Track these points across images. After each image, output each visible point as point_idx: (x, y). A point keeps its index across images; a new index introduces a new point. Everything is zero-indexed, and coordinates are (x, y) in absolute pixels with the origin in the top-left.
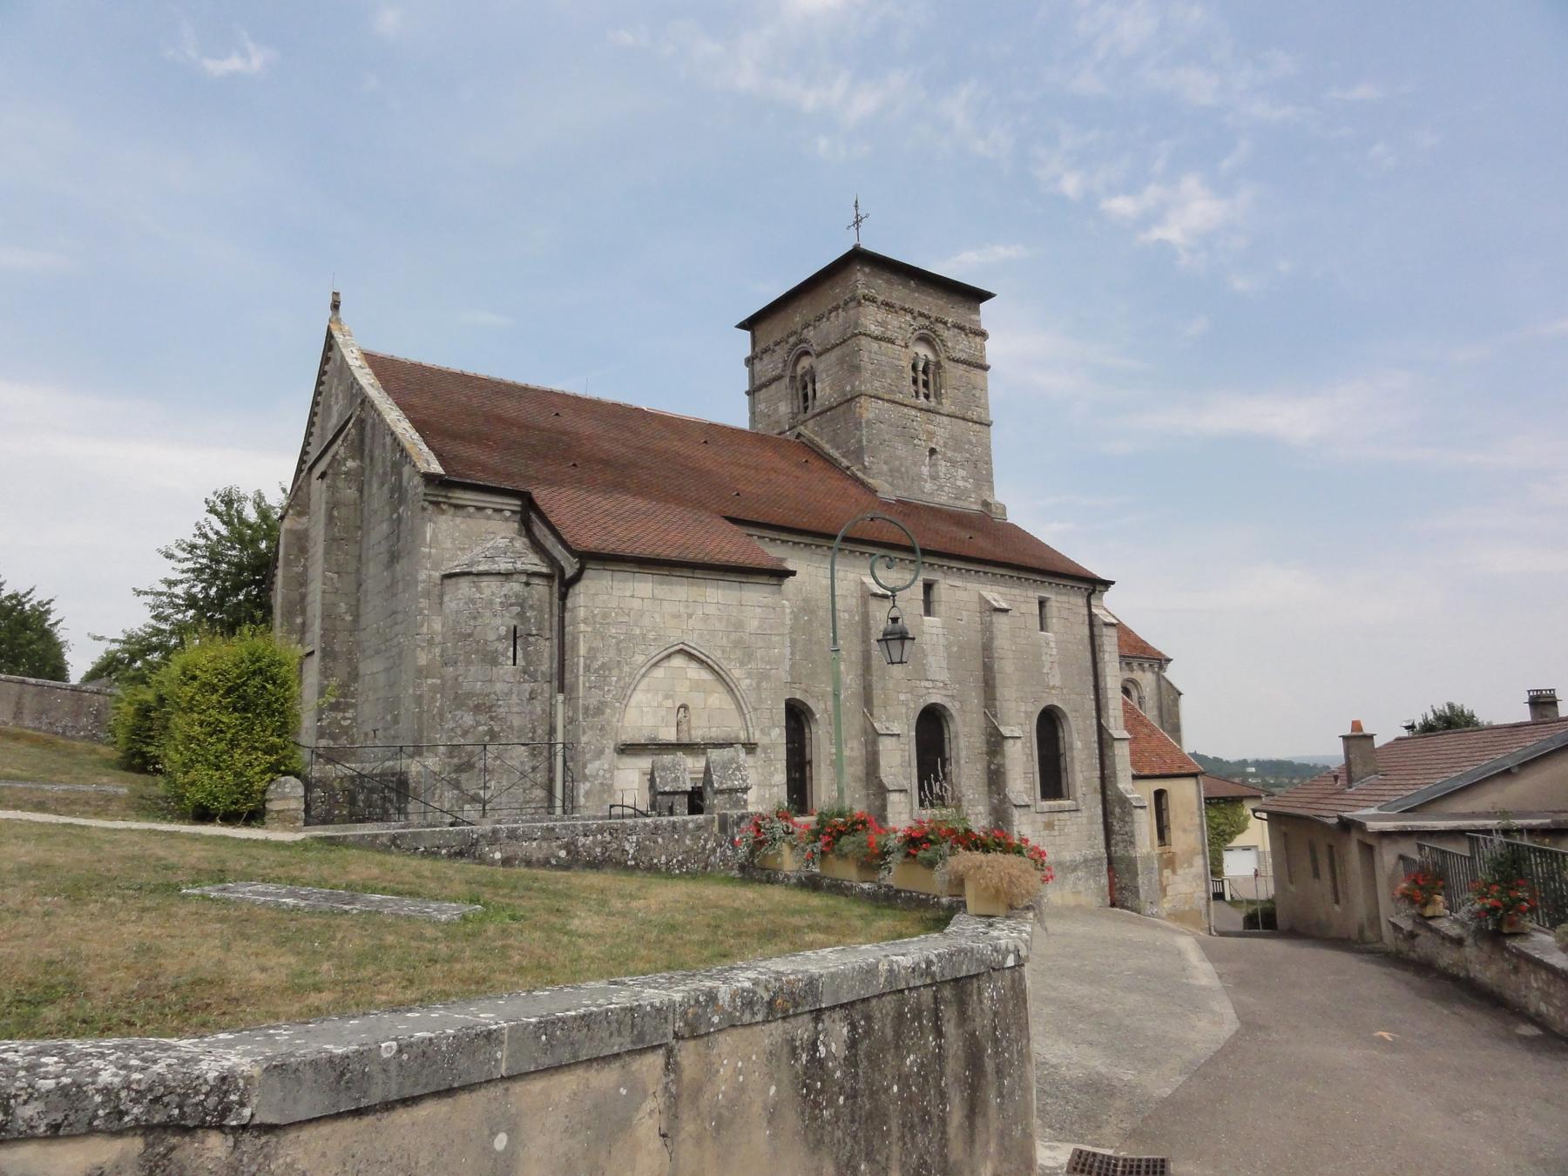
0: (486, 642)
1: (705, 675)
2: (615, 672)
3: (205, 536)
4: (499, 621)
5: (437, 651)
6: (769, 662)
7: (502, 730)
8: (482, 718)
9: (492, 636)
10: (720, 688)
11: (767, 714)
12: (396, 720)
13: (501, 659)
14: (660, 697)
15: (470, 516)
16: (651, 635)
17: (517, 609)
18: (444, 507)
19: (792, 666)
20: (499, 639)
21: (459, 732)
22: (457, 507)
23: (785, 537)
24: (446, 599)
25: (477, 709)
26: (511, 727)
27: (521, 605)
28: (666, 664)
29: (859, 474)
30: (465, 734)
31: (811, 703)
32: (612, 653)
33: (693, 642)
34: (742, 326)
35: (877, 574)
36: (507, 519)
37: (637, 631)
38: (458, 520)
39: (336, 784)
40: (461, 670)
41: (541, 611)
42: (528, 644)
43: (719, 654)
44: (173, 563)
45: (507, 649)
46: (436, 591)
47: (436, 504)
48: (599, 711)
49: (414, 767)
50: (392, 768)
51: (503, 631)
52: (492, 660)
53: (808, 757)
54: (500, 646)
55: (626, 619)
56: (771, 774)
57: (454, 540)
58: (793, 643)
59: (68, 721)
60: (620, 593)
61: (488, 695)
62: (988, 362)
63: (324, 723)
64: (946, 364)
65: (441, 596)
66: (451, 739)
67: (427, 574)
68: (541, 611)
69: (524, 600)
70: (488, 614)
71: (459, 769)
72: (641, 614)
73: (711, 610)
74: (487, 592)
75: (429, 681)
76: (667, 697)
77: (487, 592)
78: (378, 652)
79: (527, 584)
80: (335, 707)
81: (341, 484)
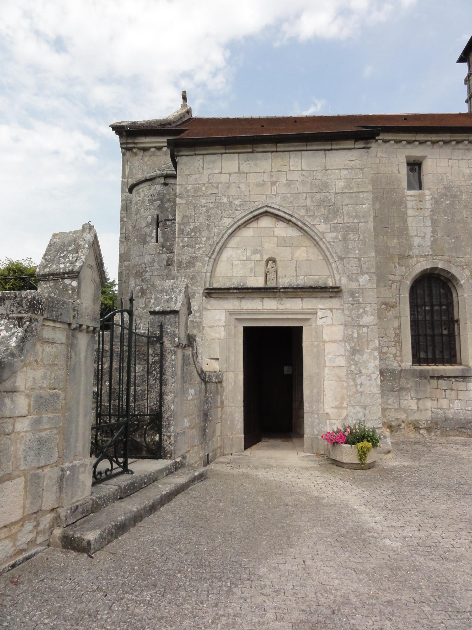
1: (292, 232)
2: (205, 233)
6: (357, 217)
7: (148, 288)
9: (144, 225)
10: (308, 243)
11: (354, 262)
13: (149, 238)
14: (249, 253)
15: (154, 154)
16: (237, 202)
17: (158, 203)
19: (434, 242)
20: (148, 226)
22: (145, 150)
23: (421, 137)
27: (161, 200)
28: (254, 225)
31: (454, 271)
32: (202, 219)
33: (276, 204)
37: (225, 200)
42: (165, 226)
43: (303, 212)
45: (152, 232)
48: (191, 263)
53: (456, 318)
54: (148, 230)
55: (215, 191)
56: (360, 316)
58: (434, 223)
60: (209, 172)
69: (164, 196)
72: (228, 185)
73: (295, 176)
76: (255, 252)
79: (165, 184)
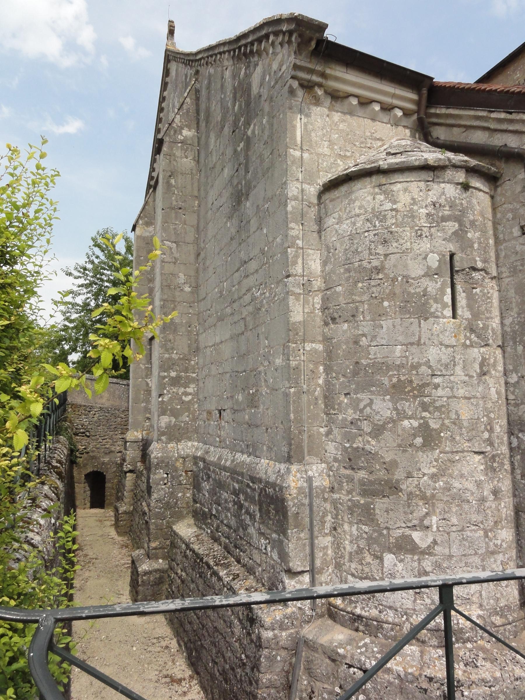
0: (407, 279)
3: (92, 262)
4: (425, 245)
5: (318, 300)
8: (408, 406)
12: (253, 402)
13: (434, 307)
17: (452, 226)
18: (320, 92)
20: (430, 274)
21: (366, 427)
24: (330, 221)
25: (399, 390)
26: (457, 422)
27: (459, 219)
30: (378, 431)
36: (396, 124)
38: (337, 116)
39: (178, 464)
40: (366, 327)
41: (484, 232)
42: (472, 285)
44: (71, 278)
46: (312, 213)
47: (308, 87)
49: (294, 480)
50: (250, 466)
51: (434, 260)
52: (419, 308)
57: (331, 143)
61: (415, 367)
63: (166, 399)
65: (320, 221)
66: (350, 438)
67: (301, 189)
68: (484, 232)
70: (408, 233)
71: (370, 490)
74: (404, 199)
75: (308, 346)
77: (404, 199)
78: (221, 319)
79: (466, 187)
80: (176, 382)
81: (178, 153)
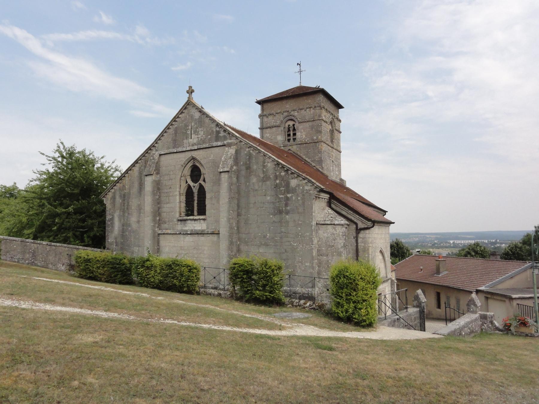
9: (340, 247)
29: (320, 170)
34: (259, 102)
35: (333, 206)
40: (330, 258)
59: (20, 256)
62: (341, 130)
64: (335, 131)
70: (338, 239)
74: (338, 231)
